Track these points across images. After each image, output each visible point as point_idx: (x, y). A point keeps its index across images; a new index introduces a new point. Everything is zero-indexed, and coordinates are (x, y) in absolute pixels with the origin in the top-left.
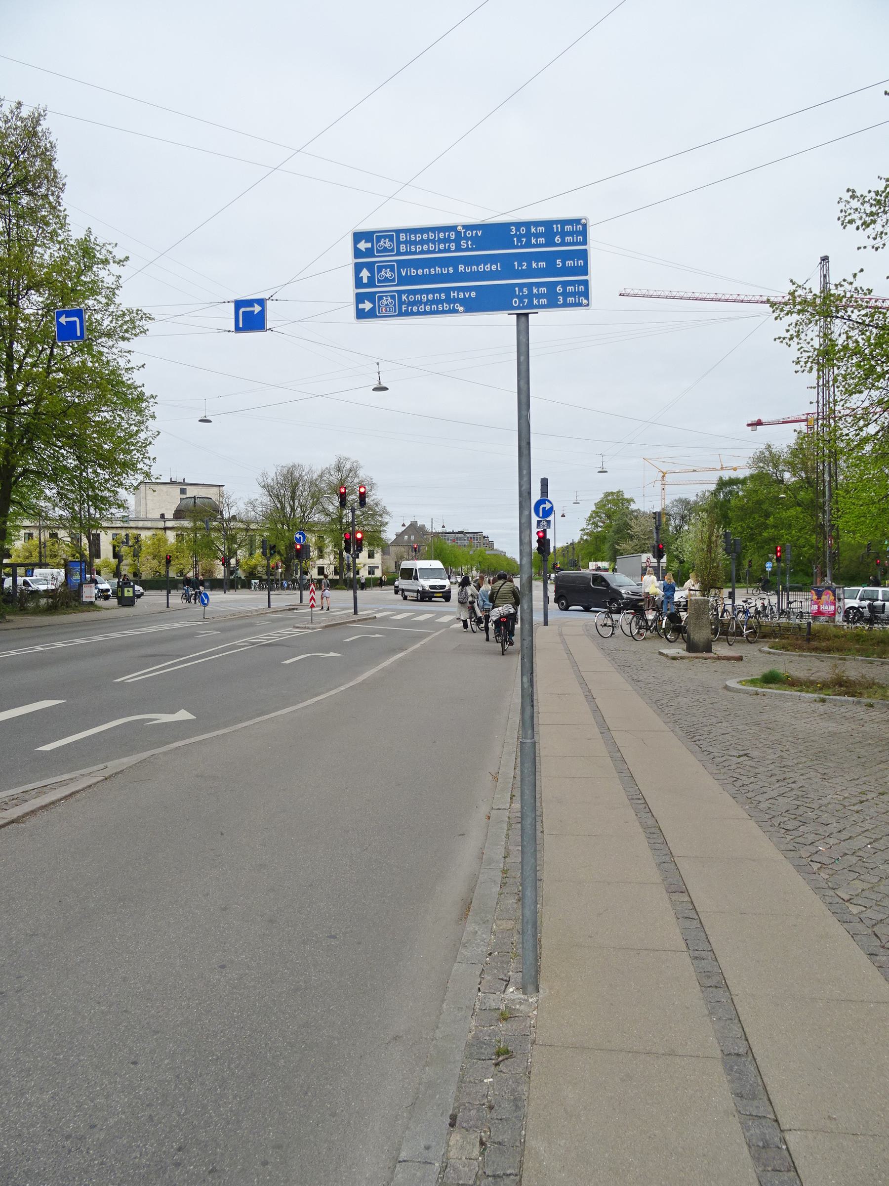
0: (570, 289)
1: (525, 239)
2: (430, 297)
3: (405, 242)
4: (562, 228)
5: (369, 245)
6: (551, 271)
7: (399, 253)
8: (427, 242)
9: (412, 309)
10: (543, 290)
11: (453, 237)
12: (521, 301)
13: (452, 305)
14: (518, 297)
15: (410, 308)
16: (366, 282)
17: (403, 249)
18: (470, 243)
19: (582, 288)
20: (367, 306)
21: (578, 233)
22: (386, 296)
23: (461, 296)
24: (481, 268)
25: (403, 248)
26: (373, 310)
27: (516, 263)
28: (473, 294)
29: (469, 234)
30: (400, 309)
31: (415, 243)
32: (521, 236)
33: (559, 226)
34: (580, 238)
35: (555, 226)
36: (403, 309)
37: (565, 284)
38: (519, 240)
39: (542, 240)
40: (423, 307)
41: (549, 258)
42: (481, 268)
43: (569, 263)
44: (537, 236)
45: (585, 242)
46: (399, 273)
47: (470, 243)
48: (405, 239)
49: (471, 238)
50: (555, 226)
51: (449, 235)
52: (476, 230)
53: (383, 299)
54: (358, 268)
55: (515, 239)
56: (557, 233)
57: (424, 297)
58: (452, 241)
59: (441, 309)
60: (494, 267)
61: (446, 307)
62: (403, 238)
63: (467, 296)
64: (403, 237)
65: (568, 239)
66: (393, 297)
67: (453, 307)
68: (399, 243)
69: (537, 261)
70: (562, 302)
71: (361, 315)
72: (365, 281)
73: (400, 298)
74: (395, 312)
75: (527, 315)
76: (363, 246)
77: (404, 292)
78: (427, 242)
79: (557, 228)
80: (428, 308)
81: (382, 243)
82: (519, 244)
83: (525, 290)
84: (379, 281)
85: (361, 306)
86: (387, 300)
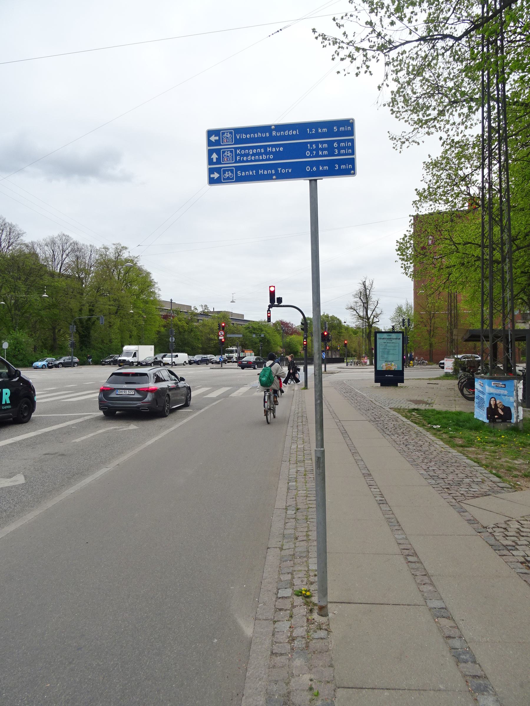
0: (342, 144)
2: (255, 151)
5: (217, 138)
6: (331, 134)
7: (236, 162)
9: (243, 159)
10: (325, 145)
13: (268, 156)
14: (310, 150)
15: (242, 158)
19: (350, 144)
20: (216, 175)
21: (349, 148)
23: (274, 150)
24: (286, 133)
26: (219, 178)
27: (308, 130)
28: (281, 149)
30: (236, 158)
36: (238, 159)
37: (339, 142)
39: (326, 152)
40: (250, 157)
42: (286, 133)
43: (342, 129)
44: (323, 150)
45: (353, 153)
46: (236, 174)
53: (226, 173)
60: (294, 132)
61: (265, 157)
63: (278, 150)
65: (342, 151)
66: (231, 152)
67: (269, 157)
71: (212, 181)
72: (215, 160)
74: (233, 161)
75: (316, 180)
76: (213, 138)
77: (238, 148)
80: (253, 158)
83: (314, 145)
85: (212, 176)
86: (228, 174)
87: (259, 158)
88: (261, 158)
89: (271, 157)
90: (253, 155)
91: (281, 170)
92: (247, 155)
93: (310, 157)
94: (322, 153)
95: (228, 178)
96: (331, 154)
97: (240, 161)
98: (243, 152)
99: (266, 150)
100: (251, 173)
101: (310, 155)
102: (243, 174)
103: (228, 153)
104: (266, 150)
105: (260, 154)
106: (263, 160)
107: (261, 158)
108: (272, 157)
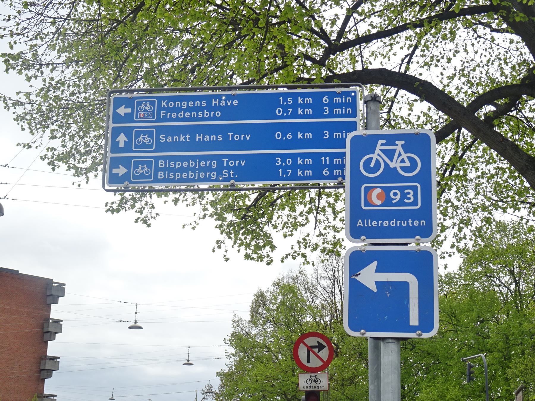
0: (337, 100)
1: (291, 171)
2: (191, 104)
3: (164, 169)
4: (331, 161)
5: (129, 110)
9: (170, 115)
10: (309, 161)
11: (215, 166)
13: (212, 113)
14: (282, 106)
15: (168, 114)
16: (123, 146)
17: (162, 162)
18: (232, 172)
20: (121, 171)
21: (347, 105)
22: (146, 102)
23: (223, 104)
28: (235, 103)
29: (232, 163)
30: (156, 175)
31: (174, 170)
33: (328, 158)
34: (349, 110)
35: (323, 158)
36: (162, 115)
39: (309, 111)
40: (182, 113)
44: (304, 106)
46: (158, 138)
47: (232, 172)
48: (163, 176)
49: (234, 168)
50: (323, 158)
51: (210, 164)
54: (116, 132)
55: (280, 170)
56: (326, 166)
57: (184, 104)
58: (214, 170)
61: (207, 114)
62: (161, 176)
63: (229, 104)
64: (161, 164)
65: (337, 110)
67: (214, 114)
69: (303, 132)
70: (328, 136)
72: (121, 145)
73: (159, 104)
74: (154, 117)
77: (164, 98)
79: (326, 160)
80: (187, 115)
82: (285, 114)
85: (115, 171)
86: (142, 169)
87: (197, 115)
88: (200, 115)
89: (218, 114)
90: (189, 109)
91: (233, 136)
92: (178, 110)
93: (282, 117)
94: (303, 112)
95: (142, 176)
97: (165, 119)
98: (171, 104)
99: (209, 103)
100: (182, 138)
101: (283, 114)
102: (170, 139)
103: (146, 106)
104: (209, 103)
105: (201, 109)
106: (203, 119)
107: (200, 115)
108: (218, 114)
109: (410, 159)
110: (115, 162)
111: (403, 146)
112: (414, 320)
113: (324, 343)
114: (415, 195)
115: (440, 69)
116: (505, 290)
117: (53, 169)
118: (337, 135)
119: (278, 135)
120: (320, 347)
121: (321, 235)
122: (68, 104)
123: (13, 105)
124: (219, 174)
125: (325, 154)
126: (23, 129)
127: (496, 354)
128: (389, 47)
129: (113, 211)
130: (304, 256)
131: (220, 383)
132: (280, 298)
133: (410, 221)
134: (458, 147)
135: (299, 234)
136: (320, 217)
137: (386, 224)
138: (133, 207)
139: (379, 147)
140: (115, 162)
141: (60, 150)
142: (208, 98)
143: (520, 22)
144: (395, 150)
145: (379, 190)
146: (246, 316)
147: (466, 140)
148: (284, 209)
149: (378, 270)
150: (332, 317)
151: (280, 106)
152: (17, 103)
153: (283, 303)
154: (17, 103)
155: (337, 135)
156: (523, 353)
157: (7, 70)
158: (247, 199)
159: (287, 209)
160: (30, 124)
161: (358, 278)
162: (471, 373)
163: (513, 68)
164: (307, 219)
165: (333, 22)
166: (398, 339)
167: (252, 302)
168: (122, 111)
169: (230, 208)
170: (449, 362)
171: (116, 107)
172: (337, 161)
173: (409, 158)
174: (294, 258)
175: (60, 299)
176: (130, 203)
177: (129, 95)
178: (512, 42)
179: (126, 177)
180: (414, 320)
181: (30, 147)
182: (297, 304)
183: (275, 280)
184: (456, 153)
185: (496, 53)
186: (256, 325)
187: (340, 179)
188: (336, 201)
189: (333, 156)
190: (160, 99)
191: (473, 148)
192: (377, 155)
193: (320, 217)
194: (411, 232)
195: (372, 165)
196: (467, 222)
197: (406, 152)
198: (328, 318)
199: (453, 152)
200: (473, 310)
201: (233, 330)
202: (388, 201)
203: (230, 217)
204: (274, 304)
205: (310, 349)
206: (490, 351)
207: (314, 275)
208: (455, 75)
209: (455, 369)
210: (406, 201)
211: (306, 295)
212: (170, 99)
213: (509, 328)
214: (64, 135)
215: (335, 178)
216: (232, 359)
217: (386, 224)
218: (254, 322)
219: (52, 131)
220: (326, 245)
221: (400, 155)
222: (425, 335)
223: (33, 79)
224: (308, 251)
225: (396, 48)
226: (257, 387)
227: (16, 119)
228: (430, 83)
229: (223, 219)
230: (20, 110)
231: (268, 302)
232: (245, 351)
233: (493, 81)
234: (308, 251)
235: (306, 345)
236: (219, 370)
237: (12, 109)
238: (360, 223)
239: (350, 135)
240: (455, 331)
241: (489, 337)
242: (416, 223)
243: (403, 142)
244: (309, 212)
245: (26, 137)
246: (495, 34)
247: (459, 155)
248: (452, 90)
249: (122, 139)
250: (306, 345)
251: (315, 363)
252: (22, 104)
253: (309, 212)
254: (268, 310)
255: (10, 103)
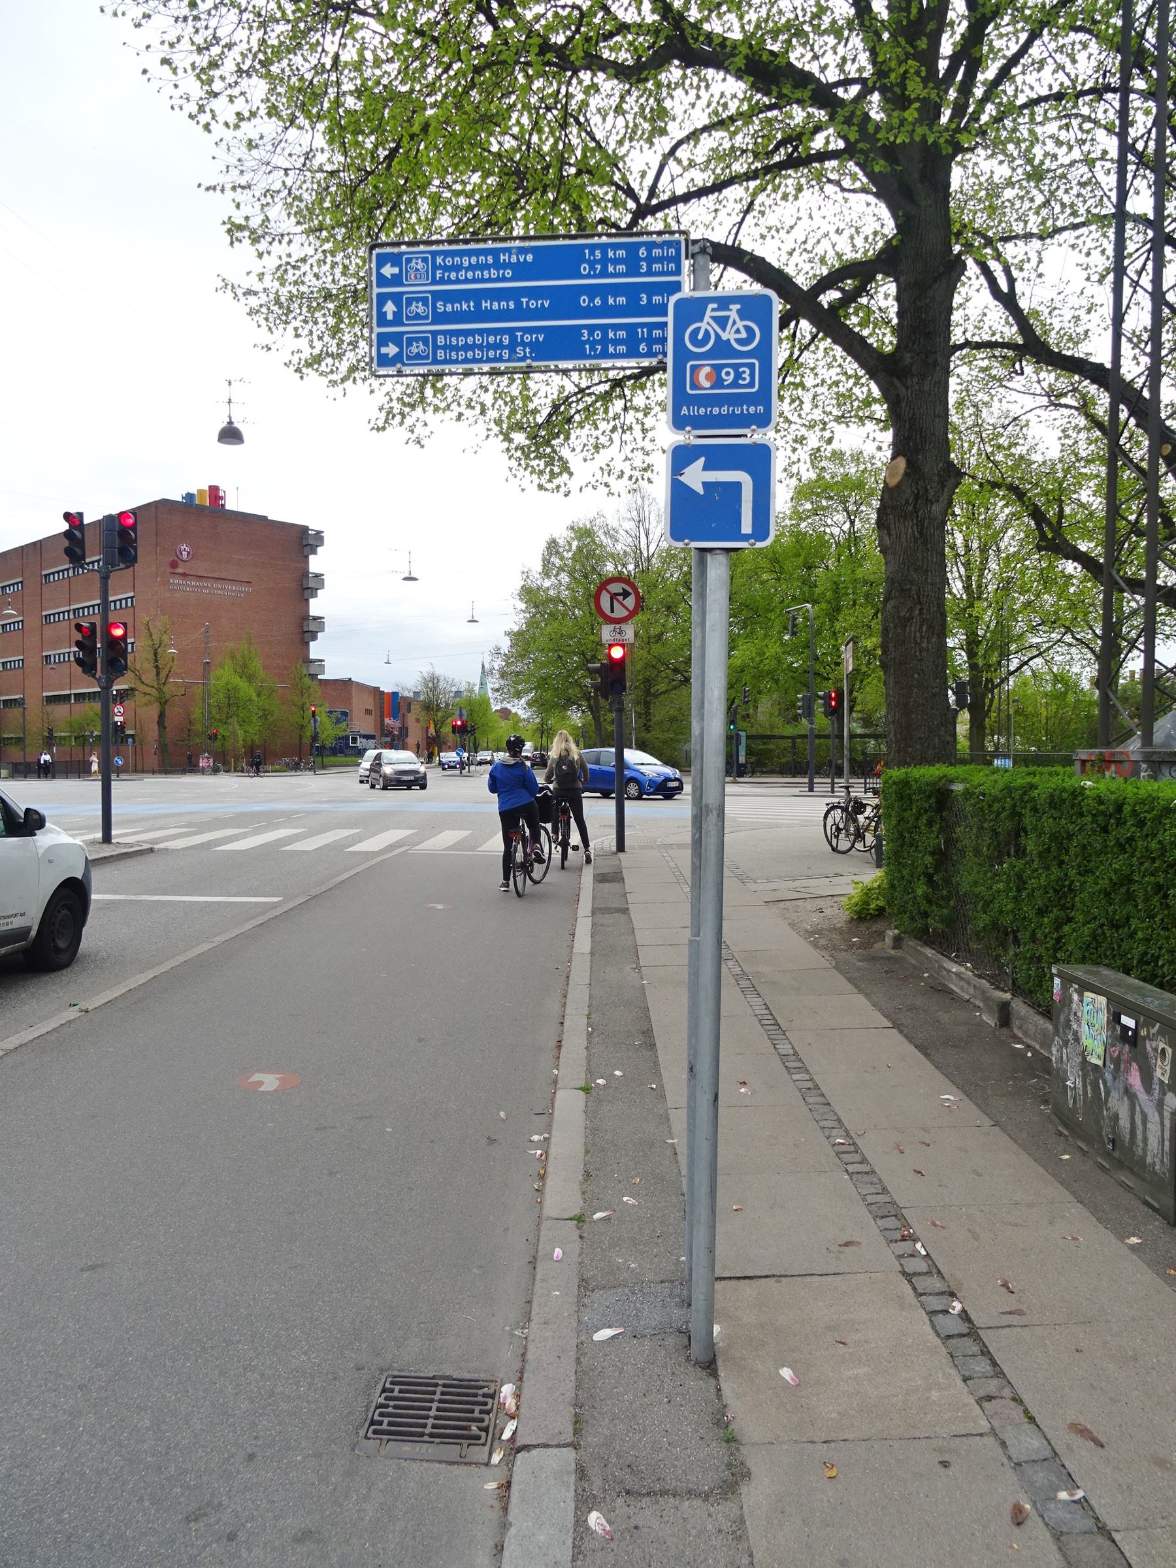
0: (657, 252)
2: (474, 260)
3: (444, 348)
4: (650, 333)
5: (396, 270)
8: (473, 347)
10: (622, 334)
11: (506, 342)
12: (592, 268)
14: (589, 262)
18: (528, 350)
20: (391, 350)
21: (670, 259)
23: (514, 259)
25: (441, 354)
28: (530, 258)
29: (527, 338)
30: (435, 354)
31: (457, 348)
32: (596, 342)
34: (672, 266)
38: (593, 348)
39: (622, 268)
41: (631, 291)
44: (616, 261)
46: (434, 307)
49: (530, 344)
52: (537, 333)
59: (486, 276)
64: (441, 340)
65: (656, 267)
66: (425, 260)
68: (436, 347)
69: (615, 296)
72: (390, 317)
73: (434, 261)
78: (473, 347)
79: (643, 333)
80: (470, 275)
81: (413, 308)
83: (598, 253)
84: (408, 318)
85: (384, 350)
90: (471, 268)
91: (527, 303)
92: (457, 268)
93: (588, 276)
95: (418, 356)
96: (633, 271)
97: (442, 281)
99: (496, 259)
102: (449, 308)
104: (496, 259)
106: (490, 280)
108: (509, 273)
109: (748, 328)
110: (383, 340)
111: (738, 311)
112: (747, 527)
113: (630, 590)
114: (752, 375)
115: (777, 243)
116: (836, 531)
117: (302, 378)
118: (657, 299)
119: (584, 301)
120: (626, 594)
121: (627, 459)
122: (312, 292)
123: (244, 294)
124: (512, 351)
125: (643, 325)
126: (259, 326)
127: (824, 606)
128: (713, 214)
129: (378, 429)
130: (607, 485)
131: (509, 643)
132: (575, 544)
133: (745, 407)
134: (793, 346)
135: (603, 457)
136: (625, 437)
137: (716, 411)
138: (402, 423)
139: (709, 313)
140: (383, 340)
141: (306, 353)
142: (495, 252)
143: (880, 172)
144: (728, 317)
145: (707, 369)
146: (537, 566)
147: (803, 337)
148: (582, 427)
149: (706, 468)
150: (637, 566)
151: (585, 261)
152: (249, 292)
153: (580, 549)
154: (249, 292)
155: (657, 299)
156: (854, 604)
157: (232, 243)
158: (538, 416)
159: (587, 427)
160: (267, 319)
161: (682, 478)
162: (794, 626)
163: (866, 238)
164: (611, 439)
165: (643, 175)
166: (728, 550)
167: (540, 557)
168: (388, 271)
169: (519, 427)
170: (769, 615)
171: (380, 265)
172: (657, 333)
173: (745, 327)
174: (594, 488)
175: (319, 549)
176: (398, 418)
177: (395, 250)
178: (868, 204)
179: (397, 359)
180: (747, 527)
181: (269, 349)
182: (594, 550)
183: (569, 523)
184: (792, 354)
185: (848, 219)
186: (549, 577)
187: (660, 357)
188: (646, 415)
189: (651, 327)
190: (434, 254)
191: (812, 348)
192: (706, 324)
193: (627, 437)
194: (745, 421)
195: (700, 337)
196: (800, 440)
197: (742, 319)
198: (631, 567)
199: (788, 353)
200: (799, 555)
201: (523, 583)
202: (718, 383)
203: (520, 438)
204: (568, 551)
205: (613, 597)
206: (815, 602)
207: (616, 517)
208: (794, 250)
209: (777, 622)
210: (740, 382)
211: (606, 540)
212: (446, 254)
213: (840, 575)
214: (311, 332)
215: (655, 355)
216: (521, 616)
217: (716, 411)
218: (546, 573)
219: (296, 329)
220: (633, 473)
221: (734, 323)
222: (759, 545)
223: (265, 255)
224: (612, 480)
225: (722, 214)
226: (551, 646)
227: (250, 314)
228: (763, 259)
229: (510, 441)
230: (254, 302)
231: (561, 550)
232: (536, 607)
233: (839, 256)
234: (612, 480)
235: (608, 592)
236: (508, 629)
237: (242, 299)
238: (684, 411)
239: (673, 299)
240: (778, 579)
241: (816, 586)
242: (752, 410)
243: (738, 306)
244: (614, 430)
245: (264, 336)
246: (846, 195)
247: (795, 356)
248: (790, 270)
249: (390, 308)
250: (608, 592)
251: (620, 612)
252: (255, 293)
253: (614, 430)
254: (562, 559)
255: (240, 292)
